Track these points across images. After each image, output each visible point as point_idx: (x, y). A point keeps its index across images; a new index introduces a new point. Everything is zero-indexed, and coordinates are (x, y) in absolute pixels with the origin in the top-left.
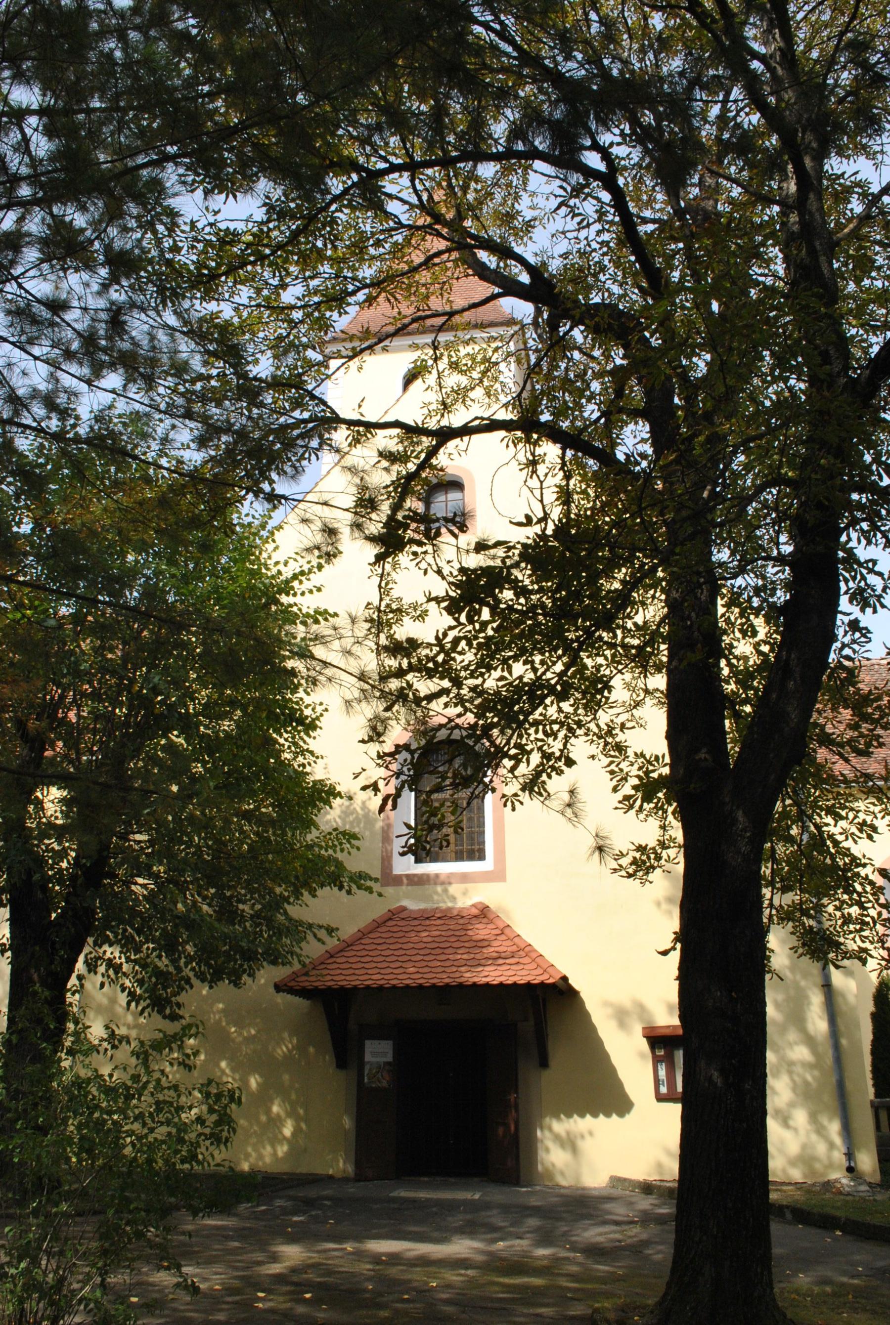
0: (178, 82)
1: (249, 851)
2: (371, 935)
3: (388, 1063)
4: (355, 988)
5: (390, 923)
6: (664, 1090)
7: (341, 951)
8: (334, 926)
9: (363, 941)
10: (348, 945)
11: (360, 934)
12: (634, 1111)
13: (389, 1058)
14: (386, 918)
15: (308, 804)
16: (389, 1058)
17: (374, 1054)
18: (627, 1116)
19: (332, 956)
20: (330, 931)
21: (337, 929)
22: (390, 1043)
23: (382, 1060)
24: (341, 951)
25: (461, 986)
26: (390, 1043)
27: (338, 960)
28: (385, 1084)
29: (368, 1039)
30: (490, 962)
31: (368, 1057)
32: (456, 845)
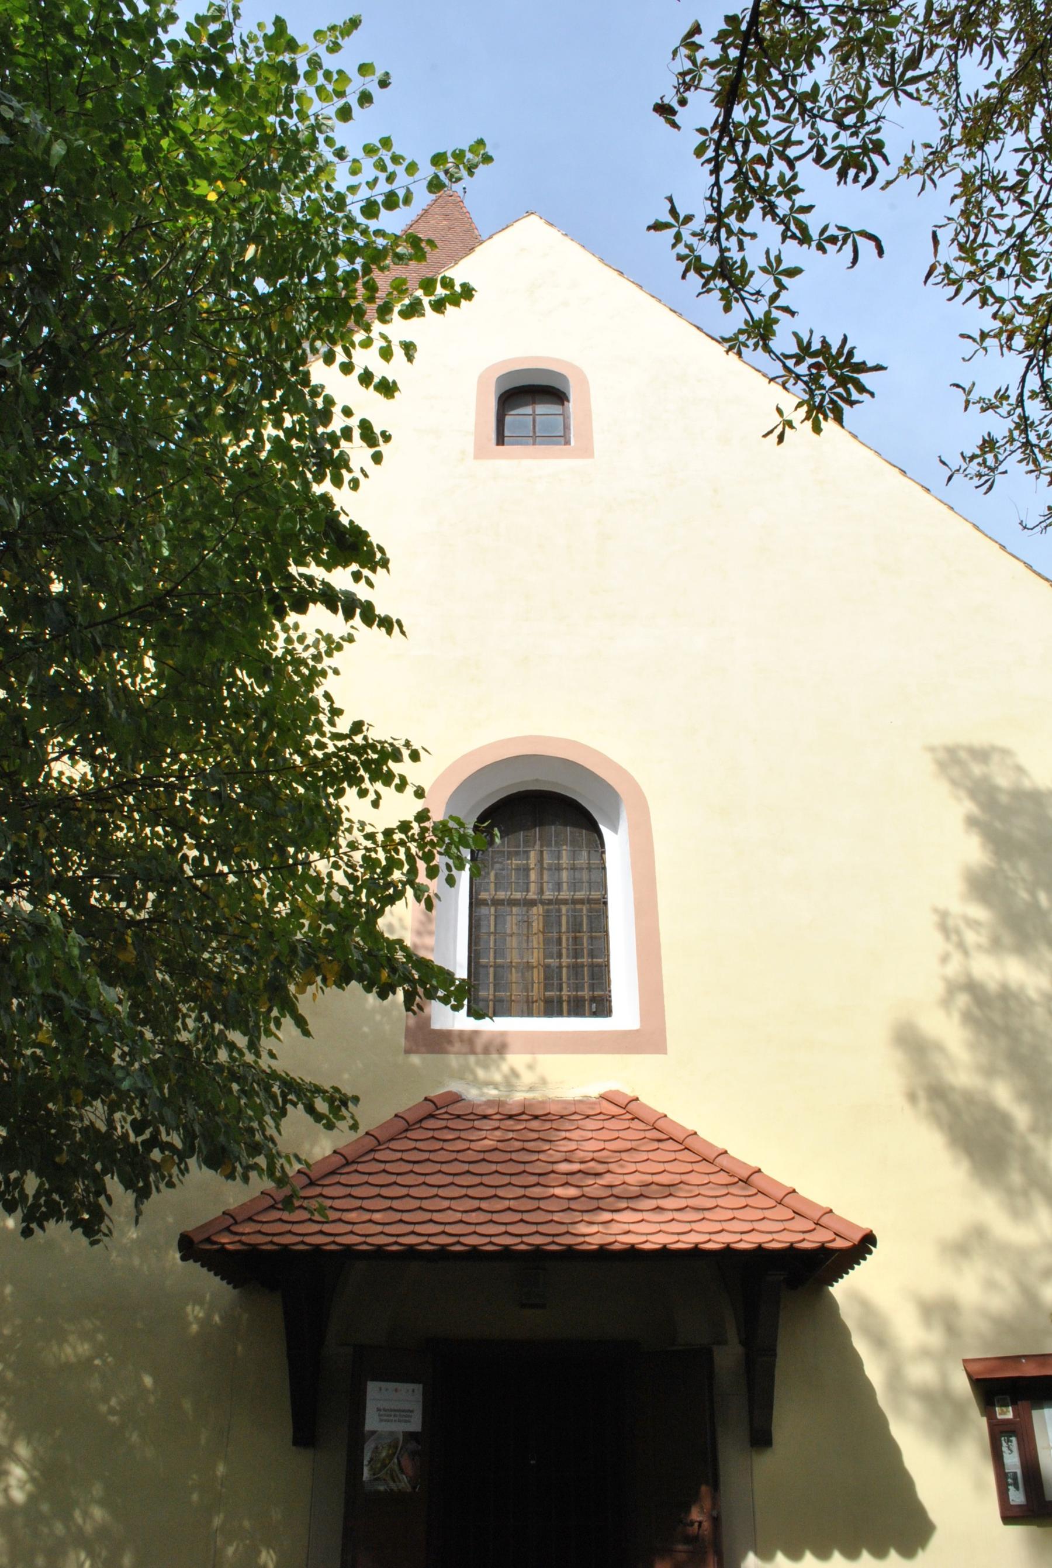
0: (138, 776)
1: (244, 468)
2: (394, 1145)
3: (410, 1436)
4: (349, 1252)
5: (430, 1123)
6: (1017, 1497)
7: (333, 1173)
8: (348, 1090)
9: (379, 1156)
10: (377, 1142)
11: (371, 1143)
12: (936, 1541)
13: (415, 1424)
14: (423, 1113)
15: (333, 778)
16: (415, 1424)
17: (385, 1414)
18: (920, 1554)
19: (312, 1183)
20: (340, 1101)
21: (356, 1099)
22: (419, 1388)
23: (400, 1427)
24: (333, 1173)
25: (571, 1254)
26: (419, 1388)
27: (327, 1191)
28: (404, 1483)
29: (373, 1379)
30: (623, 1204)
31: (372, 1422)
32: (546, 988)
